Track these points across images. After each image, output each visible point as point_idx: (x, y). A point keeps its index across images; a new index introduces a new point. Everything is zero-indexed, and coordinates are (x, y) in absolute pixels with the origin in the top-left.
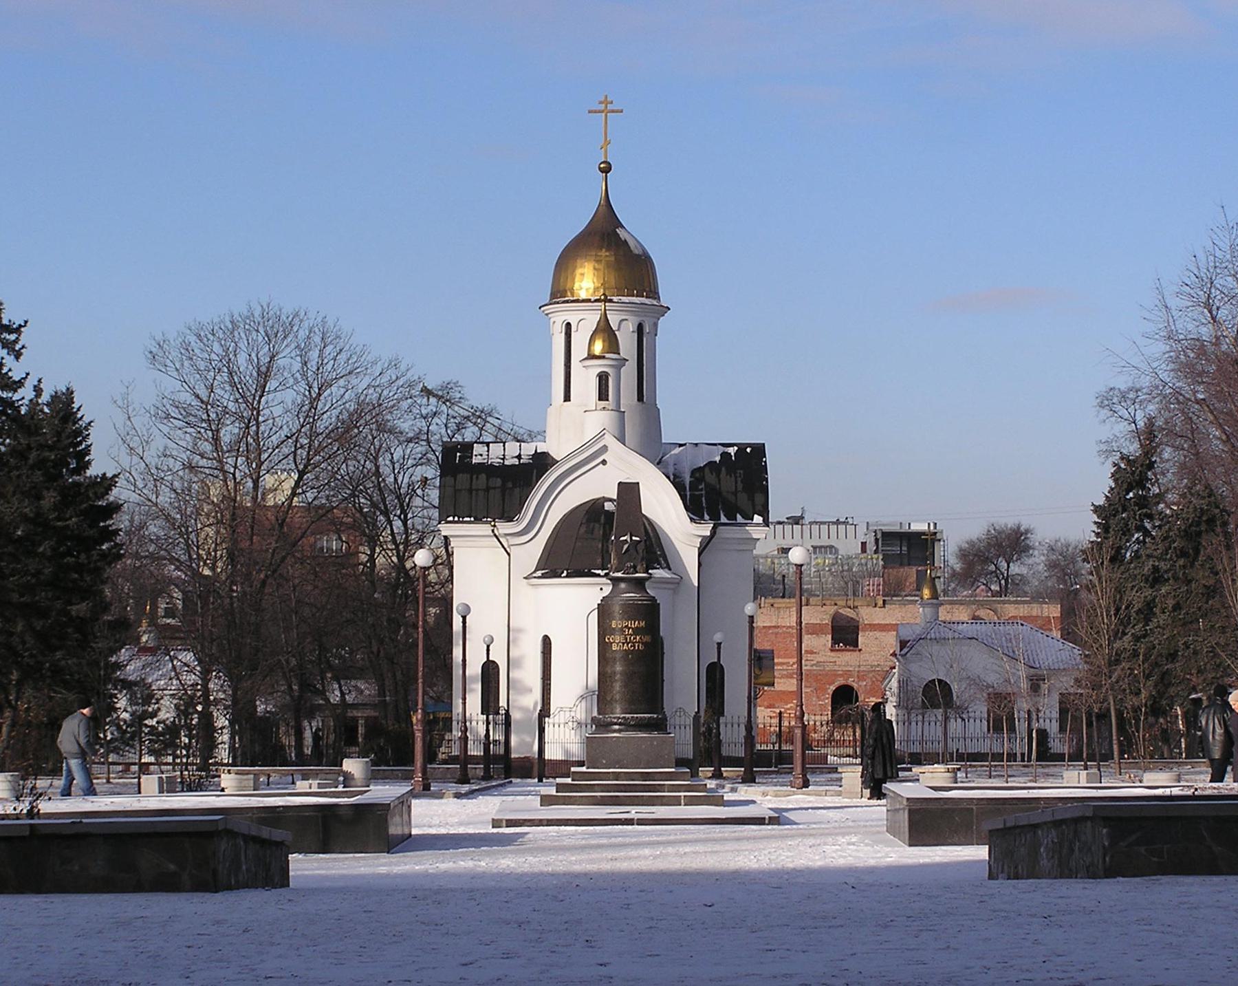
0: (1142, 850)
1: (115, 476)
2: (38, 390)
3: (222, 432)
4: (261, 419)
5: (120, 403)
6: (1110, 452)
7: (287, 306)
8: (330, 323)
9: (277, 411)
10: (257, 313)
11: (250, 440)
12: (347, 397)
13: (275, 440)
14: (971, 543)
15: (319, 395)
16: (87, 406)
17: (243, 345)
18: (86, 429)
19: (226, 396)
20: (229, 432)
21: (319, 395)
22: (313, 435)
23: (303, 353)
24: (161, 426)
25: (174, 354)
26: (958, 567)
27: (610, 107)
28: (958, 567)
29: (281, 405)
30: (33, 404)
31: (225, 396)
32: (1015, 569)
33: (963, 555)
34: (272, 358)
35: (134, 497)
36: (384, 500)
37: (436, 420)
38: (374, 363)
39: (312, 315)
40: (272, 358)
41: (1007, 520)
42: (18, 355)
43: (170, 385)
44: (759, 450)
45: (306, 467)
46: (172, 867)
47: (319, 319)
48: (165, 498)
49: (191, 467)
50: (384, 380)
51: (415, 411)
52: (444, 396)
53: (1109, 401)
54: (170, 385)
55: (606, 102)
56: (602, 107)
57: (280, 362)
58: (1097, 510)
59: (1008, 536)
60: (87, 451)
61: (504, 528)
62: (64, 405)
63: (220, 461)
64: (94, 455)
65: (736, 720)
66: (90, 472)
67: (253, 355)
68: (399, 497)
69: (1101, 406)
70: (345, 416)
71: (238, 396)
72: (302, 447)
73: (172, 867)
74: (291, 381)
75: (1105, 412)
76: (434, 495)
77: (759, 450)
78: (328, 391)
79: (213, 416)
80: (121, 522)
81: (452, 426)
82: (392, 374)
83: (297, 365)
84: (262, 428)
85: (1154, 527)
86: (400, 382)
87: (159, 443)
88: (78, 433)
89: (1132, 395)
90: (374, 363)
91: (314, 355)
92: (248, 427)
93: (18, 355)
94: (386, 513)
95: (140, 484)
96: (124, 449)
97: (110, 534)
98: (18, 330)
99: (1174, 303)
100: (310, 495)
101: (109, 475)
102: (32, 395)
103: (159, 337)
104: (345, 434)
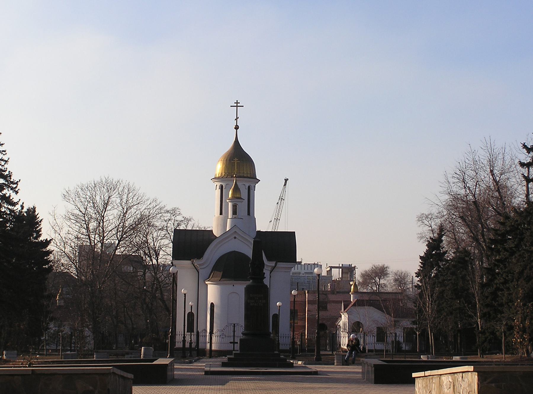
0: (493, 385)
1: (51, 240)
2: (22, 207)
3: (90, 225)
4: (104, 220)
5: (52, 214)
6: (422, 238)
7: (114, 177)
8: (131, 185)
9: (111, 217)
10: (104, 180)
11: (100, 228)
12: (137, 213)
13: (110, 228)
14: (366, 272)
15: (127, 211)
16: (41, 214)
17: (98, 192)
18: (40, 222)
19: (92, 212)
20: (93, 225)
21: (127, 211)
22: (123, 227)
23: (121, 196)
24: (67, 222)
25: (73, 195)
26: (361, 280)
27: (238, 105)
28: (361, 280)
29: (112, 216)
30: (20, 212)
31: (91, 211)
32: (382, 281)
33: (363, 276)
34: (109, 197)
35: (56, 249)
36: (149, 252)
37: (170, 222)
38: (148, 200)
39: (124, 182)
40: (109, 197)
41: (379, 263)
42: (17, 192)
43: (71, 207)
44: (291, 236)
45: (121, 238)
46: (91, 388)
47: (127, 183)
48: (68, 250)
49: (77, 238)
50: (151, 206)
51: (162, 218)
52: (174, 212)
53: (423, 218)
54: (71, 207)
55: (237, 103)
56: (236, 105)
57: (112, 199)
58: (421, 258)
59: (380, 269)
60: (40, 230)
61: (197, 262)
62: (32, 212)
63: (89, 236)
64: (43, 232)
65: (282, 335)
66: (41, 239)
67: (102, 197)
68: (155, 251)
69: (419, 221)
70: (136, 220)
71: (96, 212)
72: (120, 231)
73: (91, 388)
74: (116, 207)
75: (420, 223)
76: (170, 250)
77: (291, 236)
78: (130, 211)
79: (87, 219)
80: (51, 257)
81: (176, 224)
82: (154, 204)
83: (118, 200)
84: (105, 224)
85: (442, 265)
86: (157, 207)
87: (66, 229)
88: (37, 223)
89: (430, 217)
90: (148, 200)
91: (125, 197)
92: (99, 223)
93: (17, 192)
94: (150, 257)
95: (59, 244)
96: (53, 231)
97: (48, 262)
98: (17, 183)
99: (451, 180)
100: (122, 249)
101: (49, 240)
102: (20, 208)
103: (67, 189)
104: (134, 228)
